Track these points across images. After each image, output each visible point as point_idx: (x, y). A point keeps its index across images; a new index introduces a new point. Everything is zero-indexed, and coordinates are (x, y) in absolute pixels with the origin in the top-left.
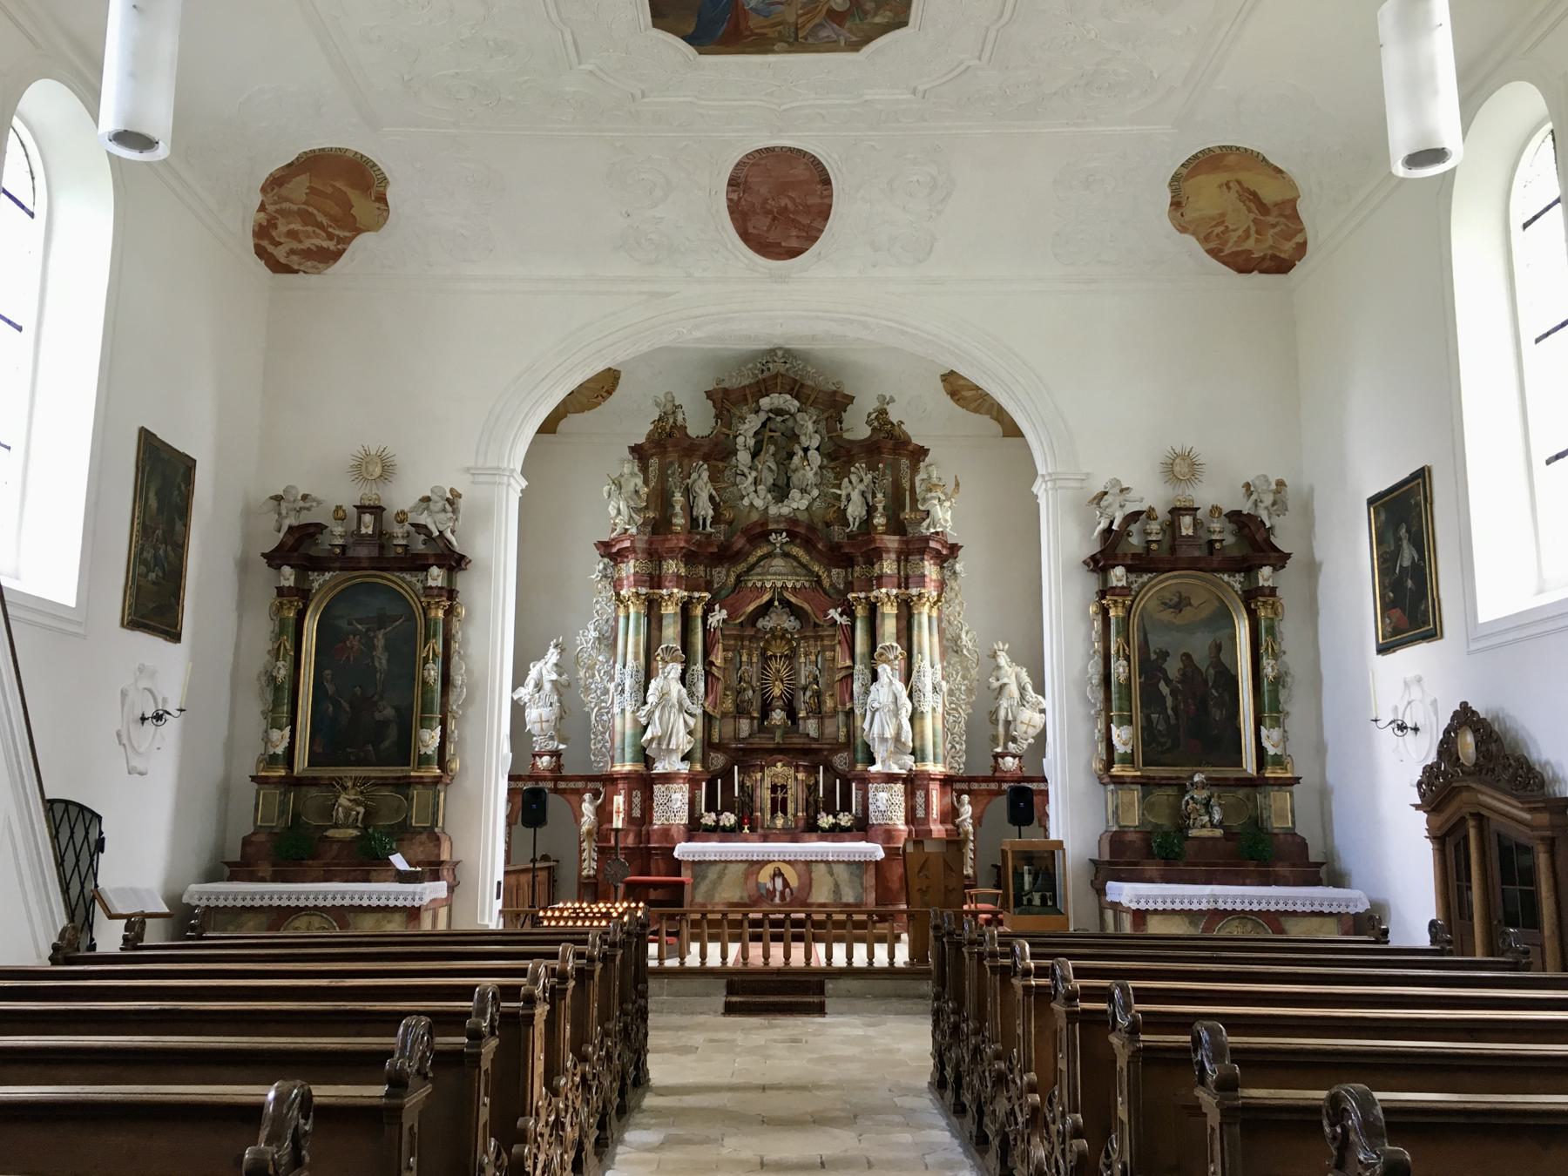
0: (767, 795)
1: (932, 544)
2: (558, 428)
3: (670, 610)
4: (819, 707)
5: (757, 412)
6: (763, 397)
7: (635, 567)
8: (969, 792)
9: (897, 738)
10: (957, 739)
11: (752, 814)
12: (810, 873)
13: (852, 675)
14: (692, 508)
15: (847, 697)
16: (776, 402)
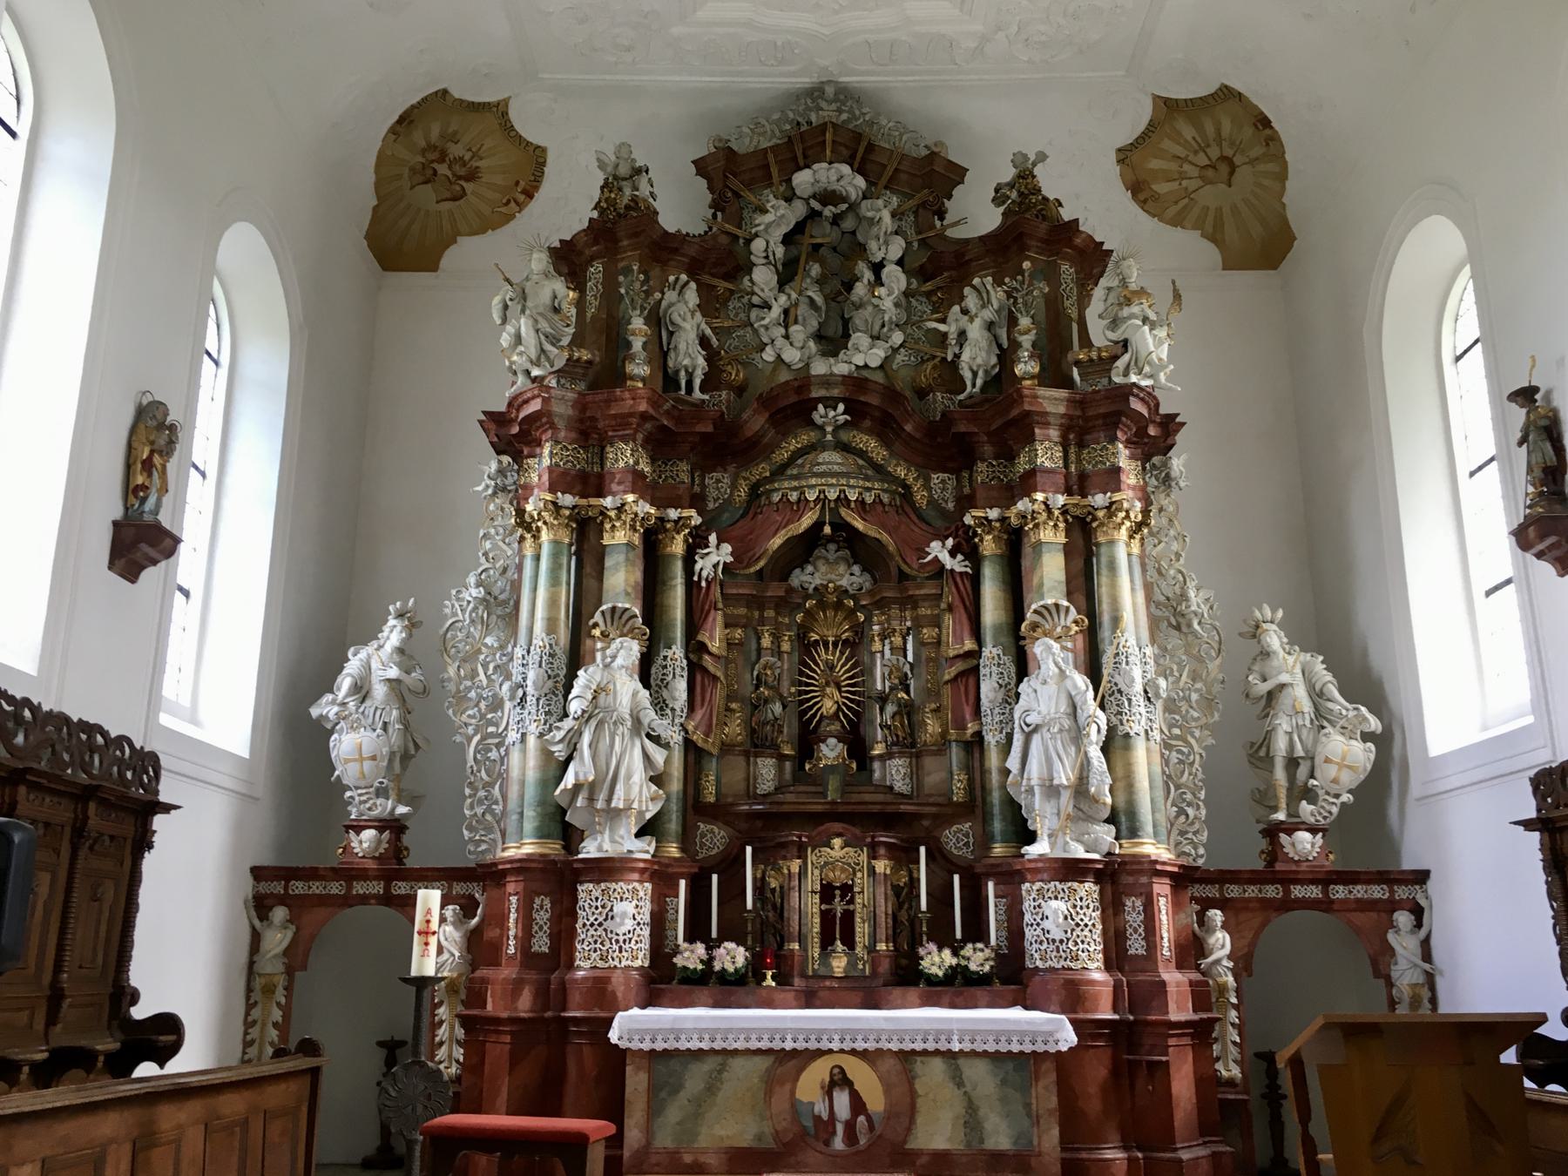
0: (813, 905)
1: (1136, 404)
2: (441, 266)
3: (618, 537)
4: (912, 735)
5: (788, 200)
6: (799, 169)
7: (552, 455)
8: (1222, 904)
9: (1081, 789)
10: (1189, 797)
11: (781, 946)
12: (910, 1078)
13: (976, 670)
14: (665, 355)
15: (968, 712)
16: (824, 179)
